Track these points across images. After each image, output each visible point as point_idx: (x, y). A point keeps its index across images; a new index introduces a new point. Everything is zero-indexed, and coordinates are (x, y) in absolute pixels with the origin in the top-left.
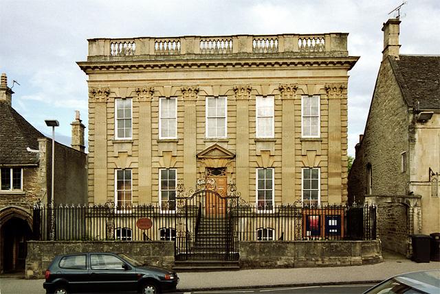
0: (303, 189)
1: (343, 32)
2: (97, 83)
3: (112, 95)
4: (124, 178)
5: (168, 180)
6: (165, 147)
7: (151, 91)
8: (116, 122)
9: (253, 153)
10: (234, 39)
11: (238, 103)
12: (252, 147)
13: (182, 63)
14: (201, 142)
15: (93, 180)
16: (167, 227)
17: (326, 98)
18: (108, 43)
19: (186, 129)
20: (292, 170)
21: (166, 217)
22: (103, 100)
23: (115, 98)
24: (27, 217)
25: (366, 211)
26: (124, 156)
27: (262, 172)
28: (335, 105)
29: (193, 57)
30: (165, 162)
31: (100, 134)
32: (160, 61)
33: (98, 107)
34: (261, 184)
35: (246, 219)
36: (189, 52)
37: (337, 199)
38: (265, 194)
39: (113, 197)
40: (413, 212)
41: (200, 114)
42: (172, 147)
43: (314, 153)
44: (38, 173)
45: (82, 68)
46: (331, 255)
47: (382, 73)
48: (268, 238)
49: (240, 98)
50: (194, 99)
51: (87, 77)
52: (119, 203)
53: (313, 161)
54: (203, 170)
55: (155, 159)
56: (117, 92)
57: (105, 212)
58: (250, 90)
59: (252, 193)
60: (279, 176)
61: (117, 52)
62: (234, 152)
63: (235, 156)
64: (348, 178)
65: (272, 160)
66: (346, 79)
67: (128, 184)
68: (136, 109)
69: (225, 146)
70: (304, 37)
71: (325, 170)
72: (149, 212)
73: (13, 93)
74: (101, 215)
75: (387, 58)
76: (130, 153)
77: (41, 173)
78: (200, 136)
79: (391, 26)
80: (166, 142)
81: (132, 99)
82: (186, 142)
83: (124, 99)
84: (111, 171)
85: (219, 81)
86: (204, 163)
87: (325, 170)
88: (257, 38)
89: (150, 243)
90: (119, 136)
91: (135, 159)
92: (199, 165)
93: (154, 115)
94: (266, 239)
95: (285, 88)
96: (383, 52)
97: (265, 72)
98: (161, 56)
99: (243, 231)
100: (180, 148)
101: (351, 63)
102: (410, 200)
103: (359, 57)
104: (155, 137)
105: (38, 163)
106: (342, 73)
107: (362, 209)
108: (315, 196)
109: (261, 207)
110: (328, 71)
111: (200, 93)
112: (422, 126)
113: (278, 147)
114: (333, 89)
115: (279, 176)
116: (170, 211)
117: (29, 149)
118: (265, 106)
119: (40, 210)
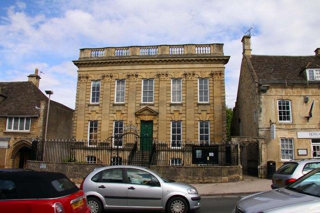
3: (90, 79)
4: (94, 125)
6: (117, 108)
8: (142, 92)
10: (130, 48)
12: (168, 108)
14: (138, 105)
18: (90, 51)
19: (130, 98)
20: (193, 122)
23: (92, 80)
25: (232, 147)
28: (217, 84)
29: (135, 57)
30: (118, 117)
31: (82, 100)
32: (117, 59)
39: (170, 138)
42: (121, 108)
43: (205, 112)
45: (75, 64)
48: (174, 164)
53: (205, 117)
54: (139, 122)
55: (111, 115)
62: (157, 111)
63: (158, 113)
64: (152, 131)
65: (180, 116)
66: (215, 67)
67: (96, 129)
69: (152, 108)
71: (213, 122)
75: (244, 57)
76: (97, 112)
77: (40, 122)
78: (138, 102)
79: (245, 39)
82: (129, 105)
84: (87, 122)
87: (213, 122)
88: (117, 49)
91: (100, 115)
93: (112, 89)
97: (143, 66)
99: (162, 159)
101: (226, 60)
102: (259, 140)
104: (112, 102)
105: (39, 115)
106: (221, 65)
108: (207, 138)
109: (173, 145)
113: (125, 108)
117: (36, 107)
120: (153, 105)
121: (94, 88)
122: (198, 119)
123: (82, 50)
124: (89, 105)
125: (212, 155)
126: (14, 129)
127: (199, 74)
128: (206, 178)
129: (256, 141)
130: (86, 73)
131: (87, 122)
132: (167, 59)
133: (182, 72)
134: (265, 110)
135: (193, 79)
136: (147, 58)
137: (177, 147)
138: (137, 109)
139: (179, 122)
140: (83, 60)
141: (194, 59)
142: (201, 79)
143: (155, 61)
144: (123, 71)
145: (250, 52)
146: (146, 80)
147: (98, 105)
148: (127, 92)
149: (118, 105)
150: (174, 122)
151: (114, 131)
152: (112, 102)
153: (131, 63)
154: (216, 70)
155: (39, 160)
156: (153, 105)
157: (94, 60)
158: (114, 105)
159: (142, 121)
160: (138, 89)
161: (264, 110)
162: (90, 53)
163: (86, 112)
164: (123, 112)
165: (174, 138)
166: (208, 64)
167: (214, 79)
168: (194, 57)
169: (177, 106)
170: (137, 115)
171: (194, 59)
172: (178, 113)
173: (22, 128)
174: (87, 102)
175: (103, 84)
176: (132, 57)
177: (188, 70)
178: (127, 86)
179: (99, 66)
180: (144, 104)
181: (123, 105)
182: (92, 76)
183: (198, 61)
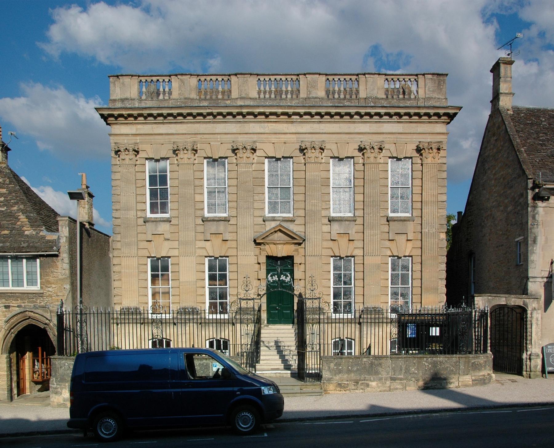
0: (390, 285)
2: (122, 138)
3: (142, 155)
5: (218, 273)
6: (213, 227)
7: (193, 150)
13: (235, 111)
20: (377, 260)
21: (216, 323)
22: (131, 162)
23: (147, 159)
27: (338, 263)
29: (248, 103)
30: (214, 248)
34: (338, 278)
36: (243, 95)
42: (221, 227)
44: (59, 264)
45: (102, 116)
50: (191, 161)
52: (154, 304)
54: (263, 260)
56: (148, 150)
57: (133, 316)
58: (323, 149)
62: (302, 235)
63: (304, 240)
68: (175, 175)
70: (350, 77)
73: (9, 150)
74: (369, 321)
75: (496, 111)
76: (168, 236)
79: (502, 67)
80: (214, 220)
81: (168, 161)
83: (157, 161)
85: (283, 136)
91: (175, 244)
93: (197, 182)
94: (351, 353)
95: (367, 147)
96: (491, 102)
97: (342, 125)
104: (199, 213)
110: (422, 125)
111: (258, 153)
113: (233, 228)
114: (183, 150)
118: (340, 174)
120: (292, 221)
121: (153, 179)
122: (389, 253)
126: (12, 286)
131: (143, 261)
134: (543, 238)
135: (319, 160)
138: (257, 228)
147: (168, 221)
148: (234, 190)
149: (213, 220)
152: (199, 213)
154: (429, 138)
156: (292, 221)
158: (205, 220)
159: (269, 257)
161: (541, 240)
163: (141, 237)
164: (227, 236)
167: (308, 160)
172: (346, 239)
173: (18, 282)
174: (140, 214)
175: (175, 168)
176: (240, 103)
177: (370, 136)
178: (234, 175)
180: (273, 219)
181: (226, 220)
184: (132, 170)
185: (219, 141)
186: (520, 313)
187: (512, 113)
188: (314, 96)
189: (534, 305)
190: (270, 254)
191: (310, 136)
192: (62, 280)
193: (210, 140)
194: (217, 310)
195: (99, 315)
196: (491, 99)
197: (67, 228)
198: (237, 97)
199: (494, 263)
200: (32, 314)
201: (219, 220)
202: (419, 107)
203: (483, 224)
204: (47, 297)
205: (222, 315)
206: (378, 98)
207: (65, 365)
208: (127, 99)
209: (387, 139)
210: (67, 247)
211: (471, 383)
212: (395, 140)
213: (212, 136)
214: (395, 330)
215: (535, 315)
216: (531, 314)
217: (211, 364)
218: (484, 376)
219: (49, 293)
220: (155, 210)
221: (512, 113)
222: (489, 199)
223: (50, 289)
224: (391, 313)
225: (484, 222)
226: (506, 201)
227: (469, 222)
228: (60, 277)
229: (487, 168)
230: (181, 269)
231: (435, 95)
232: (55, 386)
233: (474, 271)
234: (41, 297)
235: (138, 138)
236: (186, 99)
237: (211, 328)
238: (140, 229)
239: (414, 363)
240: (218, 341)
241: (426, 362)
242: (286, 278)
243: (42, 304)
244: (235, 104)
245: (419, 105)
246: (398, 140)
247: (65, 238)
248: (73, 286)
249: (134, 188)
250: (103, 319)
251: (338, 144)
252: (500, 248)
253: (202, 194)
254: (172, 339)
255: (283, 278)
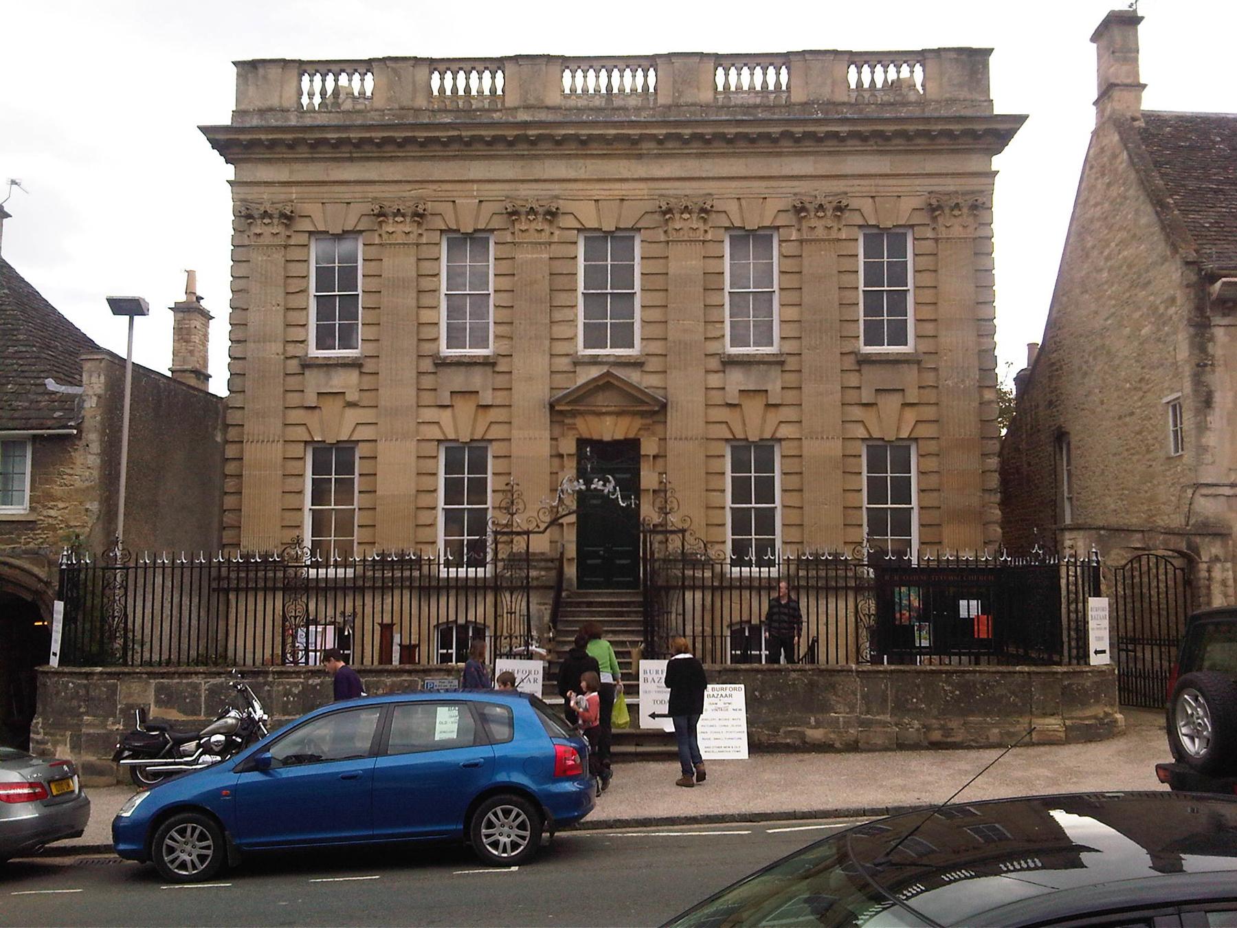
1: (974, 46)
4: (335, 461)
6: (457, 380)
9: (717, 397)
11: (673, 250)
12: (714, 380)
14: (563, 363)
15: (984, 455)
16: (461, 621)
17: (930, 234)
23: (310, 233)
24: (36, 592)
26: (331, 408)
29: (543, 116)
30: (459, 424)
31: (263, 339)
33: (258, 258)
34: (741, 491)
35: (698, 595)
36: (532, 101)
37: (969, 546)
38: (753, 527)
40: (1210, 579)
41: (561, 282)
42: (477, 379)
43: (894, 401)
45: (215, 144)
46: (972, 713)
47: (1095, 166)
49: (673, 236)
50: (544, 237)
51: (229, 171)
53: (890, 421)
54: (568, 446)
55: (429, 414)
59: (715, 517)
60: (793, 466)
61: (317, 100)
62: (659, 395)
63: (664, 406)
65: (773, 417)
67: (345, 488)
69: (634, 377)
72: (407, 573)
76: (352, 396)
77: (85, 465)
78: (561, 348)
82: (519, 365)
85: (617, 185)
86: (573, 427)
89: (298, 674)
90: (319, 346)
92: (556, 433)
98: (446, 111)
100: (501, 381)
101: (1000, 132)
102: (1198, 540)
103: (1027, 117)
104: (427, 348)
105: (78, 427)
107: (1057, 567)
108: (903, 527)
112: (1226, 321)
113: (791, 379)
115: (793, 466)
116: (472, 570)
117: (51, 385)
119: (79, 570)
121: (324, 277)
122: (861, 432)
123: (249, 69)
124: (307, 364)
125: (963, 603)
127: (867, 205)
128: (954, 724)
129: (1183, 546)
130: (280, 194)
132: (708, 131)
133: (914, 194)
136: (607, 124)
137: (759, 565)
139: (765, 450)
140: (255, 121)
141: (843, 129)
142: (875, 237)
143: (642, 138)
144: (476, 187)
145: (1138, 100)
146: (596, 238)
147: (355, 364)
149: (459, 363)
150: (741, 449)
151: (866, 529)
153: (522, 149)
155: (114, 664)
156: (636, 364)
157: (322, 128)
158: (442, 364)
159: (582, 443)
160: (560, 281)
162: (294, 84)
163: (294, 399)
164: (487, 397)
165: (740, 524)
166: (452, 164)
168: (844, 121)
169: (754, 369)
170: (561, 410)
171: (844, 129)
174: (292, 350)
175: (373, 252)
176: (523, 116)
179: (351, 159)
180: (594, 361)
181: (487, 363)
182: (313, 209)
183: (863, 138)
184: (278, 257)
185: (475, 197)
186: (1182, 569)
187: (1143, 125)
188: (690, 101)
189: (1214, 551)
190: (586, 435)
191: (678, 184)
192: (85, 491)
193: (455, 194)
194: (328, 560)
195: (178, 572)
196: (1096, 97)
197: (102, 378)
198: (516, 104)
199: (1115, 455)
200: (6, 568)
201: (471, 363)
202: (927, 120)
203: (1085, 367)
204: (43, 529)
205: (453, 570)
206: (834, 104)
207: (67, 686)
208: (271, 109)
209: (853, 189)
210: (98, 418)
211: (1063, 735)
212: (873, 189)
213: (459, 186)
214: (869, 605)
215: (1217, 574)
216: (1209, 571)
217: (420, 683)
218: (1095, 717)
219: (50, 520)
220: (329, 342)
221: (1143, 125)
222: (1096, 313)
223: (52, 513)
224: (732, 565)
225: (1086, 362)
226: (1137, 315)
227: (1053, 364)
228: (78, 484)
229: (1089, 245)
230: (379, 467)
231: (964, 94)
232: (39, 737)
233: (1069, 471)
234: (32, 530)
235: (294, 189)
236: (402, 109)
237: (443, 601)
238: (293, 382)
239: (918, 686)
240: (462, 630)
241: (945, 682)
242: (604, 485)
243: (31, 545)
244: (511, 119)
245: (927, 114)
246: (881, 189)
247: (95, 399)
248: (109, 505)
249: (283, 295)
250: (187, 580)
251: (743, 202)
252: (1127, 419)
253: (436, 308)
254: (396, 620)
255: (597, 484)
